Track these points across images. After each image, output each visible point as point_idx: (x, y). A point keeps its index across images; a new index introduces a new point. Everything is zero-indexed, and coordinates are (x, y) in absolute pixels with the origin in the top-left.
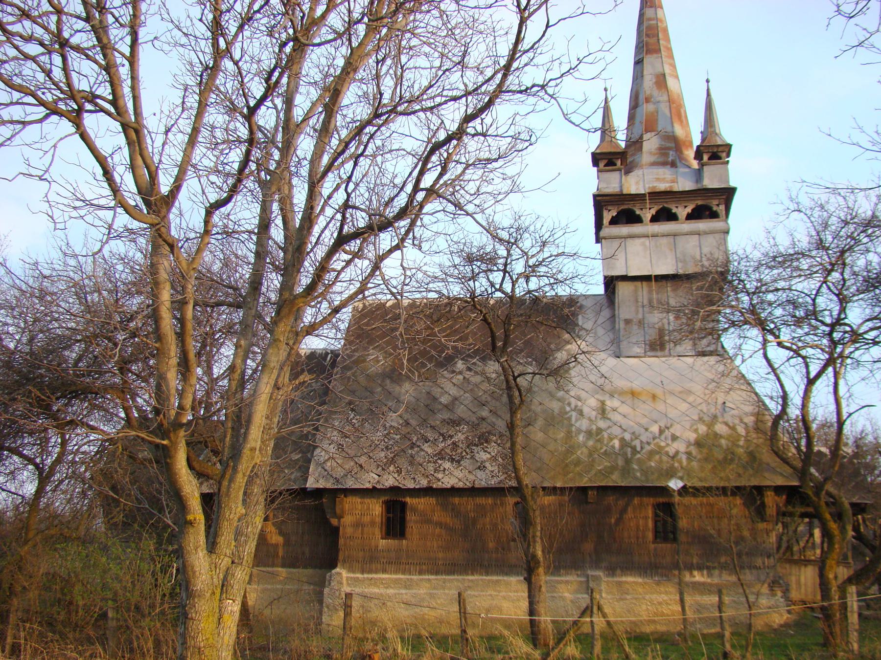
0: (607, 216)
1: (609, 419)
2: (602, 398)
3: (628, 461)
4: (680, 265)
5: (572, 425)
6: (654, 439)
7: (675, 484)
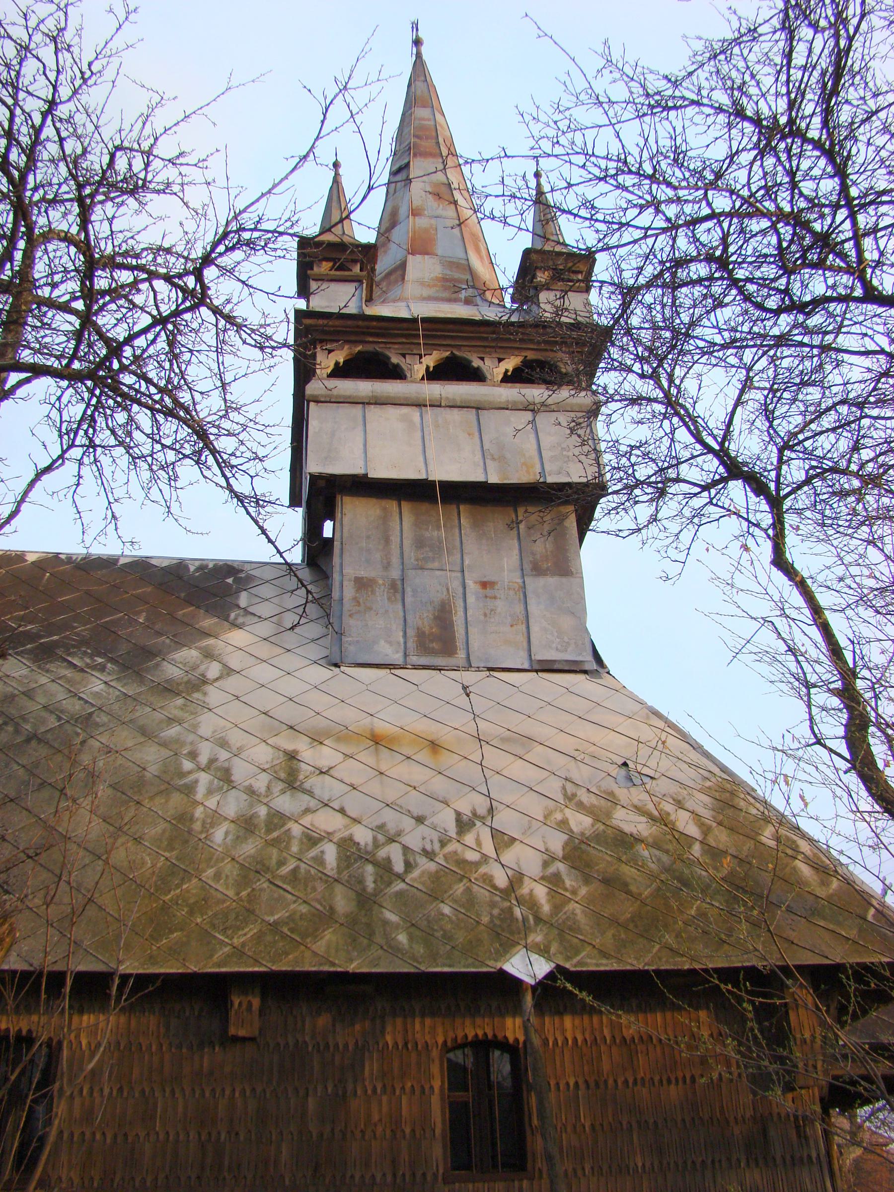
0: (326, 361)
1: (310, 793)
2: (290, 747)
3: (366, 901)
4: (492, 465)
5: (196, 803)
6: (443, 844)
7: (527, 967)
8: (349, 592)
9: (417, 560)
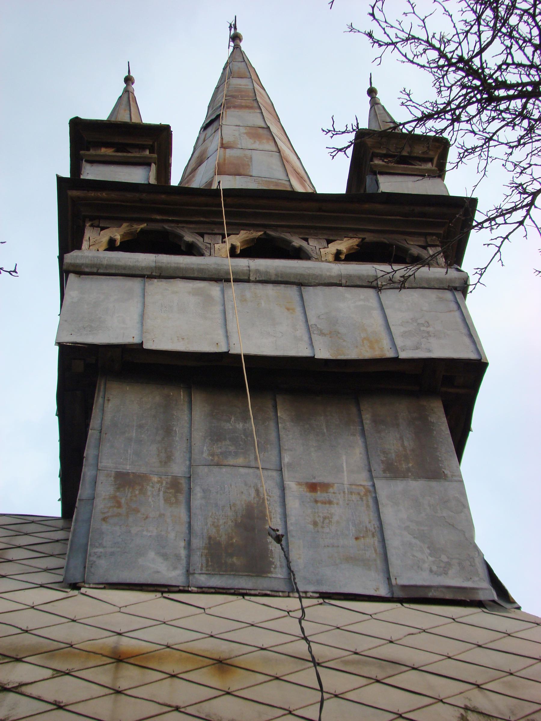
8: (105, 489)
9: (213, 455)
